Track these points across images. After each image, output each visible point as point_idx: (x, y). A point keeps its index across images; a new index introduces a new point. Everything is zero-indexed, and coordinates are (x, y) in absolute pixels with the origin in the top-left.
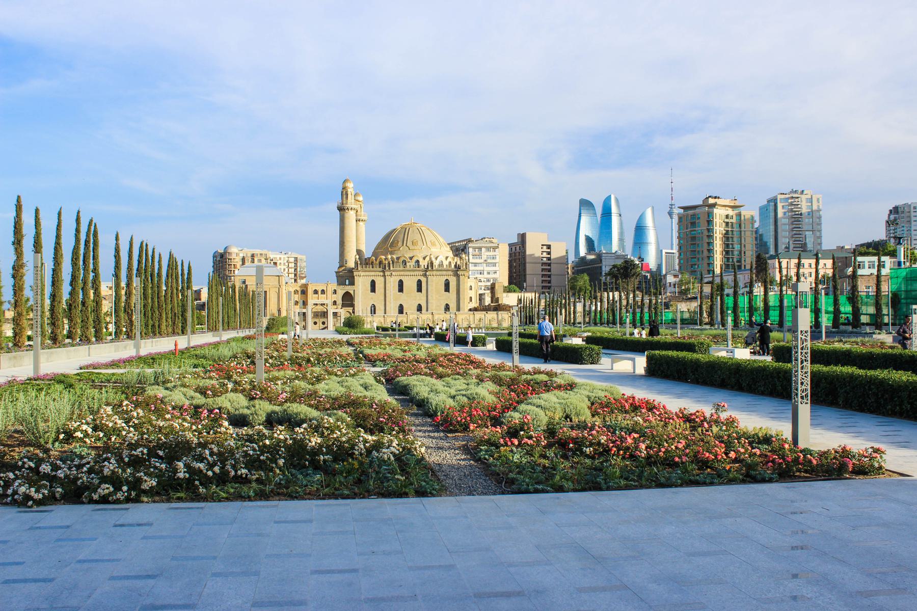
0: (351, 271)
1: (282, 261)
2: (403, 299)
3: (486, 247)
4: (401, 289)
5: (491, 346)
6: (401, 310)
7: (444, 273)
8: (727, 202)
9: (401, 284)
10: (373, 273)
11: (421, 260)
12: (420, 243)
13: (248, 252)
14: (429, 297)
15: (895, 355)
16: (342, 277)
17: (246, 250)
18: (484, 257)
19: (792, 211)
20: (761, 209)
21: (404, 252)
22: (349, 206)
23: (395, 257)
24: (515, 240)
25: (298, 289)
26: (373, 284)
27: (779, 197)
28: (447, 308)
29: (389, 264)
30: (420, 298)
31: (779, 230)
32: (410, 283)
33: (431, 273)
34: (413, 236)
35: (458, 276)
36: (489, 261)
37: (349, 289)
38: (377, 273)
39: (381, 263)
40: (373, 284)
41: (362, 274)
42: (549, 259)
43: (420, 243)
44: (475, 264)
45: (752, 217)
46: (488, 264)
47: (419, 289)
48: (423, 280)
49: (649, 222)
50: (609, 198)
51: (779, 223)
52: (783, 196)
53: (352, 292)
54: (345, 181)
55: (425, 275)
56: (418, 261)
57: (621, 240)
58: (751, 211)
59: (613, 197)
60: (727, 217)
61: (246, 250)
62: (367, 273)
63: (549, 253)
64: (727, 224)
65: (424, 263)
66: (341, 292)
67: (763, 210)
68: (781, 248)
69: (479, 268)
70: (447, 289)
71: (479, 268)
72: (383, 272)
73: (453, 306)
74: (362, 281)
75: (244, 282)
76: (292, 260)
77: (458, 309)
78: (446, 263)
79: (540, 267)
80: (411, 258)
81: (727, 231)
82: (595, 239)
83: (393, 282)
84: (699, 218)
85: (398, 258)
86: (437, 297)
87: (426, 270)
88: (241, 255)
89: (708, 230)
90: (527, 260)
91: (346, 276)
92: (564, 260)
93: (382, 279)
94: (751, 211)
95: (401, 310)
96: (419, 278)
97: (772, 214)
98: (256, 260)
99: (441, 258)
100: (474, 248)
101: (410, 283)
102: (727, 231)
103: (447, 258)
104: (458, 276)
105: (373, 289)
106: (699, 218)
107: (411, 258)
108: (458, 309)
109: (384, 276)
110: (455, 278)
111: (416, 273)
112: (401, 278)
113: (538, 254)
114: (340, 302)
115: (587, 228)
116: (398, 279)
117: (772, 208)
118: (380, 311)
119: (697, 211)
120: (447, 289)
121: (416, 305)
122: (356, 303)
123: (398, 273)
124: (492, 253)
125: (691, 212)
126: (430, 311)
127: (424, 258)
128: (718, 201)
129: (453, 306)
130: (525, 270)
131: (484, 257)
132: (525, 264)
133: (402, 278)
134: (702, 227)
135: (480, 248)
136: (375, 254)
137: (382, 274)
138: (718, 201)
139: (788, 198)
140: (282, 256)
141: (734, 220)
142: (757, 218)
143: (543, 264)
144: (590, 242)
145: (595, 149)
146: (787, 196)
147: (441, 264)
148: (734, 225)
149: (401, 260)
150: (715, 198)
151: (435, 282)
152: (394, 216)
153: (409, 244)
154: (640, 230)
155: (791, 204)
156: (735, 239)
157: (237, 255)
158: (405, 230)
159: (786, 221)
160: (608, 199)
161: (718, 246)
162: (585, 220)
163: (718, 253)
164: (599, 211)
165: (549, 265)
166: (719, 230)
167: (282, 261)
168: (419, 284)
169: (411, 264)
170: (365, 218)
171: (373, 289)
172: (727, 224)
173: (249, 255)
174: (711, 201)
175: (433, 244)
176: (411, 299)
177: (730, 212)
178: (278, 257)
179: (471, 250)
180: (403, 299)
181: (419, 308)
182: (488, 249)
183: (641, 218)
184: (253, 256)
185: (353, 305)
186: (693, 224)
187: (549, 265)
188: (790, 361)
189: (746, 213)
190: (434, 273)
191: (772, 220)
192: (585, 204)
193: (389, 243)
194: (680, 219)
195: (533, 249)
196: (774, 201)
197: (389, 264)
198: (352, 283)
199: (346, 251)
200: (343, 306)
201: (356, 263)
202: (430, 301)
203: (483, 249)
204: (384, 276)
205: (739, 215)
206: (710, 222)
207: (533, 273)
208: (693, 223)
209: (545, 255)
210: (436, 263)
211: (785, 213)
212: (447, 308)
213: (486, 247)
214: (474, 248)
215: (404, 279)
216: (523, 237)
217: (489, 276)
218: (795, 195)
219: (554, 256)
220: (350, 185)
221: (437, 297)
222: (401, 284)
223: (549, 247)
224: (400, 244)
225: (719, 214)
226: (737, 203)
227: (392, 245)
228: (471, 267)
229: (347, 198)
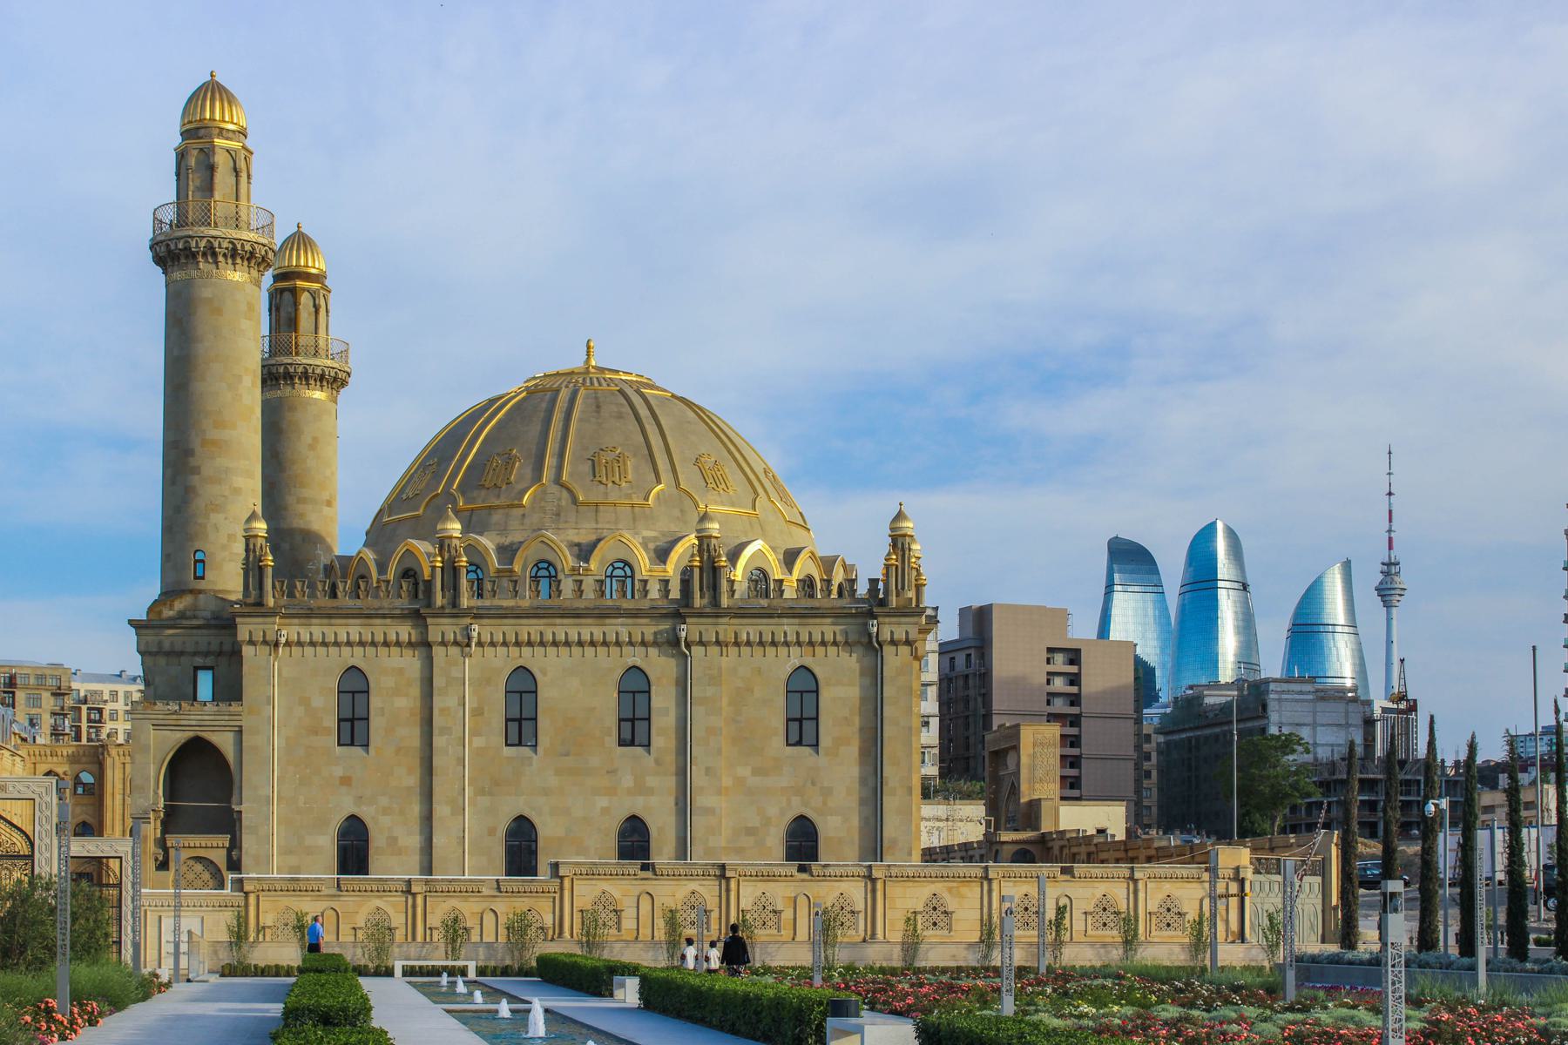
0: (223, 622)
4: (521, 725)
5: (629, 993)
6: (522, 848)
7: (788, 628)
9: (522, 692)
10: (354, 630)
11: (643, 563)
14: (697, 777)
23: (488, 543)
26: (354, 692)
28: (803, 843)
32: (577, 685)
35: (872, 647)
37: (204, 716)
38: (379, 630)
41: (289, 631)
42: (1075, 700)
47: (633, 728)
49: (1335, 608)
50: (1208, 532)
53: (224, 741)
62: (317, 630)
63: (1074, 680)
72: (417, 618)
73: (838, 829)
77: (874, 846)
80: (584, 552)
83: (472, 679)
87: (680, 611)
95: (522, 848)
96: (634, 657)
101: (577, 685)
103: (790, 558)
104: (872, 647)
105: (353, 727)
108: (874, 846)
110: (850, 662)
111: (618, 628)
112: (527, 657)
116: (502, 662)
118: (393, 861)
121: (614, 824)
122: (248, 808)
123: (508, 629)
126: (698, 858)
127: (662, 555)
133: (532, 658)
136: (381, 533)
137: (405, 631)
147: (760, 579)
160: (1205, 536)
165: (1075, 721)
168: (635, 688)
171: (353, 727)
181: (634, 841)
183: (1312, 597)
185: (228, 823)
187: (1075, 721)
188: (1379, 984)
190: (727, 628)
192: (1130, 558)
198: (230, 690)
200: (172, 821)
201: (253, 569)
204: (426, 645)
209: (1059, 684)
212: (803, 843)
215: (549, 666)
222: (522, 692)
224: (520, 470)
229: (208, 188)
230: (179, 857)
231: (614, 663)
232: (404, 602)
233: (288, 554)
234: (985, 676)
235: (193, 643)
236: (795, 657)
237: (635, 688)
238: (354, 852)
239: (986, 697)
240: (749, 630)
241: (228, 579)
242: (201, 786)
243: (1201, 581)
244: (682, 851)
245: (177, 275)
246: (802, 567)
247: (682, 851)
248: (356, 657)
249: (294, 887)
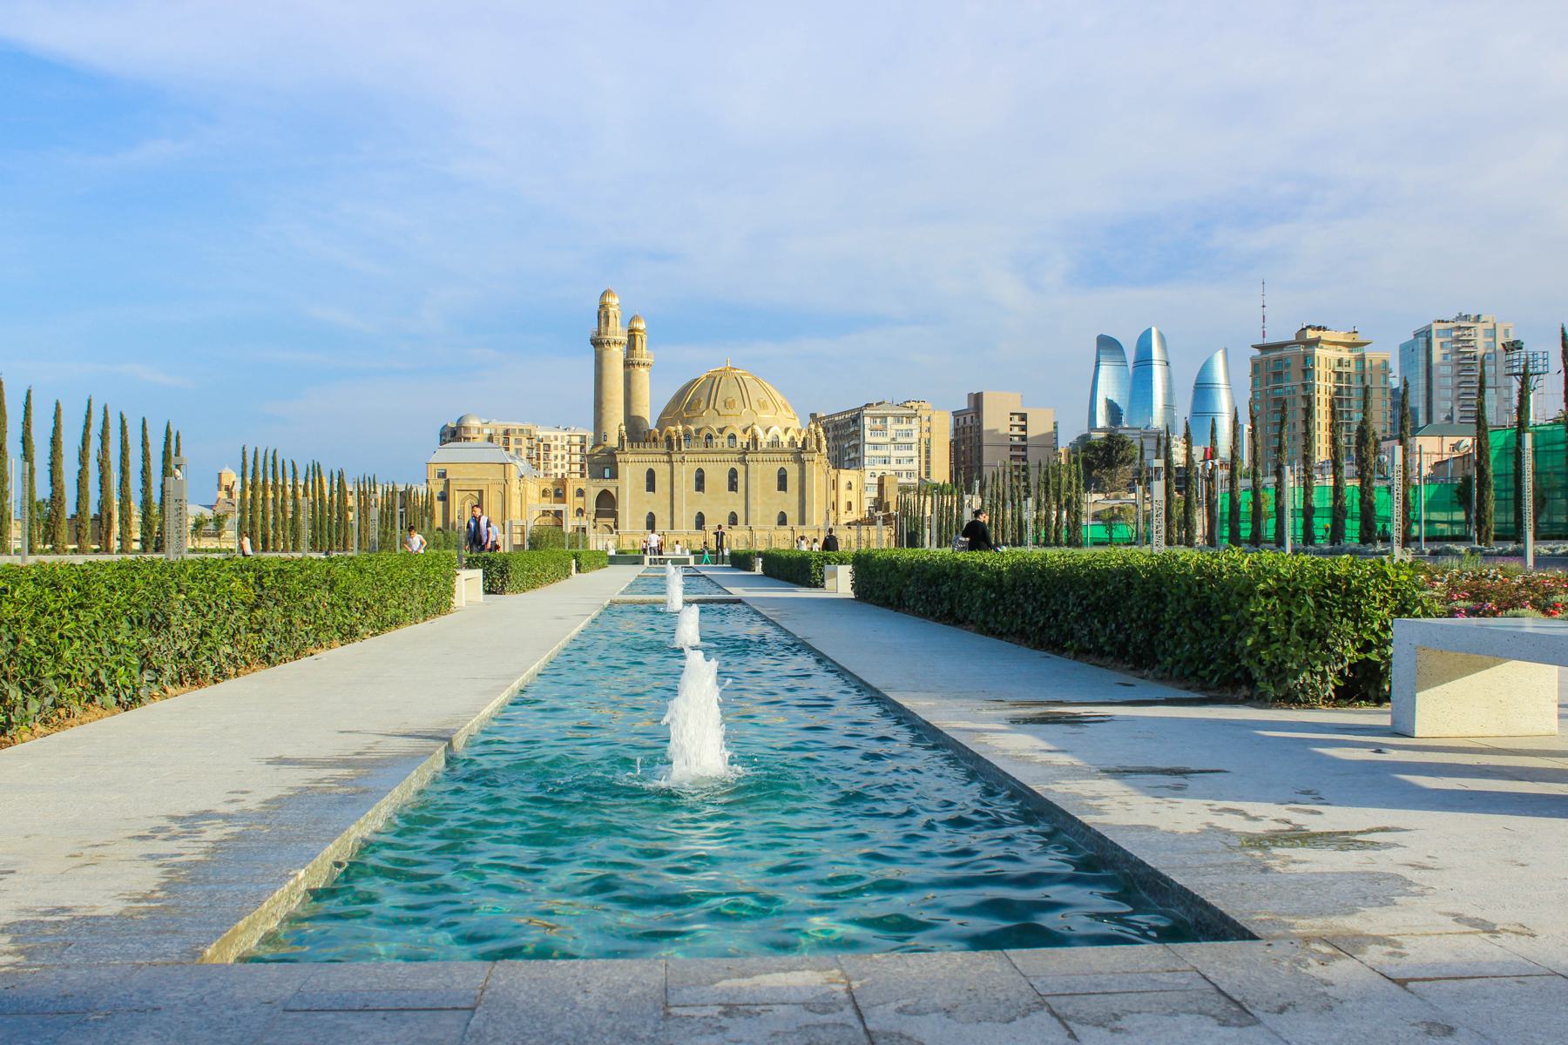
0: (612, 454)
1: (559, 443)
2: (704, 503)
3: (894, 416)
5: (841, 582)
7: (778, 456)
8: (1340, 336)
10: (651, 457)
11: (739, 434)
12: (738, 403)
13: (499, 426)
14: (751, 500)
15: (1128, 573)
16: (598, 464)
17: (494, 422)
18: (891, 433)
19: (1458, 351)
20: (1403, 348)
21: (709, 421)
22: (611, 337)
23: (692, 428)
24: (963, 405)
25: (550, 487)
26: (651, 475)
27: (1435, 327)
28: (783, 520)
29: (679, 440)
30: (735, 503)
31: (1435, 387)
32: (716, 475)
33: (754, 457)
34: (727, 390)
35: (801, 463)
36: (900, 440)
38: (658, 457)
39: (669, 439)
40: (651, 475)
41: (631, 458)
42: (1024, 438)
43: (738, 403)
44: (876, 446)
45: (1385, 363)
46: (898, 446)
47: (733, 486)
48: (740, 468)
49: (1219, 375)
50: (1148, 333)
51: (1434, 375)
52: (1442, 326)
53: (613, 491)
54: (604, 295)
55: (743, 461)
56: (733, 437)
57: (1169, 407)
58: (1384, 352)
59: (1154, 331)
60: (1340, 362)
61: (494, 422)
62: (640, 457)
63: (1024, 428)
64: (1339, 375)
65: (743, 439)
66: (593, 492)
67: (1406, 351)
68: (1439, 417)
69: (883, 452)
70: (782, 485)
71: (883, 452)
72: (669, 454)
73: (792, 516)
74: (631, 471)
75: (443, 475)
76: (576, 440)
78: (785, 439)
79: (1007, 453)
80: (721, 431)
81: (1340, 388)
82: (1123, 406)
84: (1288, 366)
85: (698, 431)
86: (765, 502)
87: (745, 451)
88: (487, 431)
89: (1305, 386)
90: (985, 441)
91: (602, 463)
92: (1050, 441)
93: (667, 467)
94: (1384, 352)
97: (1422, 358)
98: (512, 440)
99: (776, 430)
100: (874, 417)
101: (716, 475)
102: (1340, 388)
103: (786, 430)
104: (801, 463)
105: (651, 486)
106: (1288, 366)
107: (721, 431)
109: (671, 462)
110: (796, 466)
112: (701, 465)
113: (1004, 429)
114: (591, 507)
115: (1110, 386)
116: (695, 467)
117: (1422, 347)
119: (1286, 351)
120: (782, 485)
122: (619, 510)
123: (696, 457)
124: (904, 426)
125: (1274, 355)
127: (745, 431)
128: (1324, 335)
129: (792, 516)
130: (980, 458)
131: (891, 433)
132: (980, 447)
134: (1293, 381)
135: (884, 418)
136: (661, 424)
137: (666, 458)
138: (1324, 335)
139: (1452, 329)
140: (559, 434)
141: (1352, 369)
142: (1395, 366)
143: (1013, 447)
144: (1114, 410)
145: (1123, 248)
146: (1450, 325)
148: (1353, 379)
149: (728, 432)
150: (1319, 328)
151: (762, 474)
152: (696, 362)
153: (755, 405)
154: (1203, 389)
155: (1457, 340)
156: (1354, 403)
157: (479, 431)
158: (713, 382)
159: (1447, 370)
160: (1147, 335)
161: (1323, 414)
162: (1106, 372)
163: (1323, 427)
164: (1131, 357)
165: (1024, 448)
166: (1323, 388)
167: (559, 443)
168: (733, 474)
169: (721, 441)
170: (650, 361)
171: (651, 486)
172: (1339, 375)
173: (501, 432)
174: (1311, 334)
175: (763, 406)
176: (718, 504)
177: (1346, 354)
178: (552, 434)
179: (867, 420)
180: (704, 503)
182: (898, 418)
183: (1206, 369)
184: (507, 433)
185: (614, 515)
186: (1278, 375)
187: (1024, 448)
189: (1373, 355)
190: (760, 456)
191: (1422, 369)
192: (1108, 345)
193: (684, 405)
194: (1256, 366)
195: (996, 421)
196: (1426, 334)
197: (679, 440)
198: (614, 475)
199: (605, 419)
200: (598, 514)
201: (621, 439)
202: (751, 507)
203: (890, 420)
204: (671, 462)
205: (1362, 359)
206: (1307, 372)
207: (994, 460)
208: (1279, 371)
209: (1016, 431)
210: (764, 439)
211: (1445, 356)
212: (783, 520)
213: (894, 416)
214: (874, 417)
215: (706, 467)
216: (977, 400)
217: (898, 467)
218: (1463, 324)
219: (1032, 433)
220: (613, 301)
221: (765, 502)
223: (1023, 417)
224: (703, 405)
225: (1325, 357)
226: (1359, 339)
227: (688, 408)
228: (868, 451)
229: (607, 323)
230: (600, 526)
231: (727, 467)
232: (665, 450)
233: (635, 432)
234: (980, 426)
235: (602, 463)
236: (780, 465)
237: (733, 474)
238: (651, 524)
239: (980, 437)
240: (766, 457)
241: (613, 441)
242: (607, 505)
243: (1144, 361)
244: (1429, 419)
245: (621, 727)
246: (790, 433)
247: (1429, 419)
248: (651, 466)
249: (632, 533)
